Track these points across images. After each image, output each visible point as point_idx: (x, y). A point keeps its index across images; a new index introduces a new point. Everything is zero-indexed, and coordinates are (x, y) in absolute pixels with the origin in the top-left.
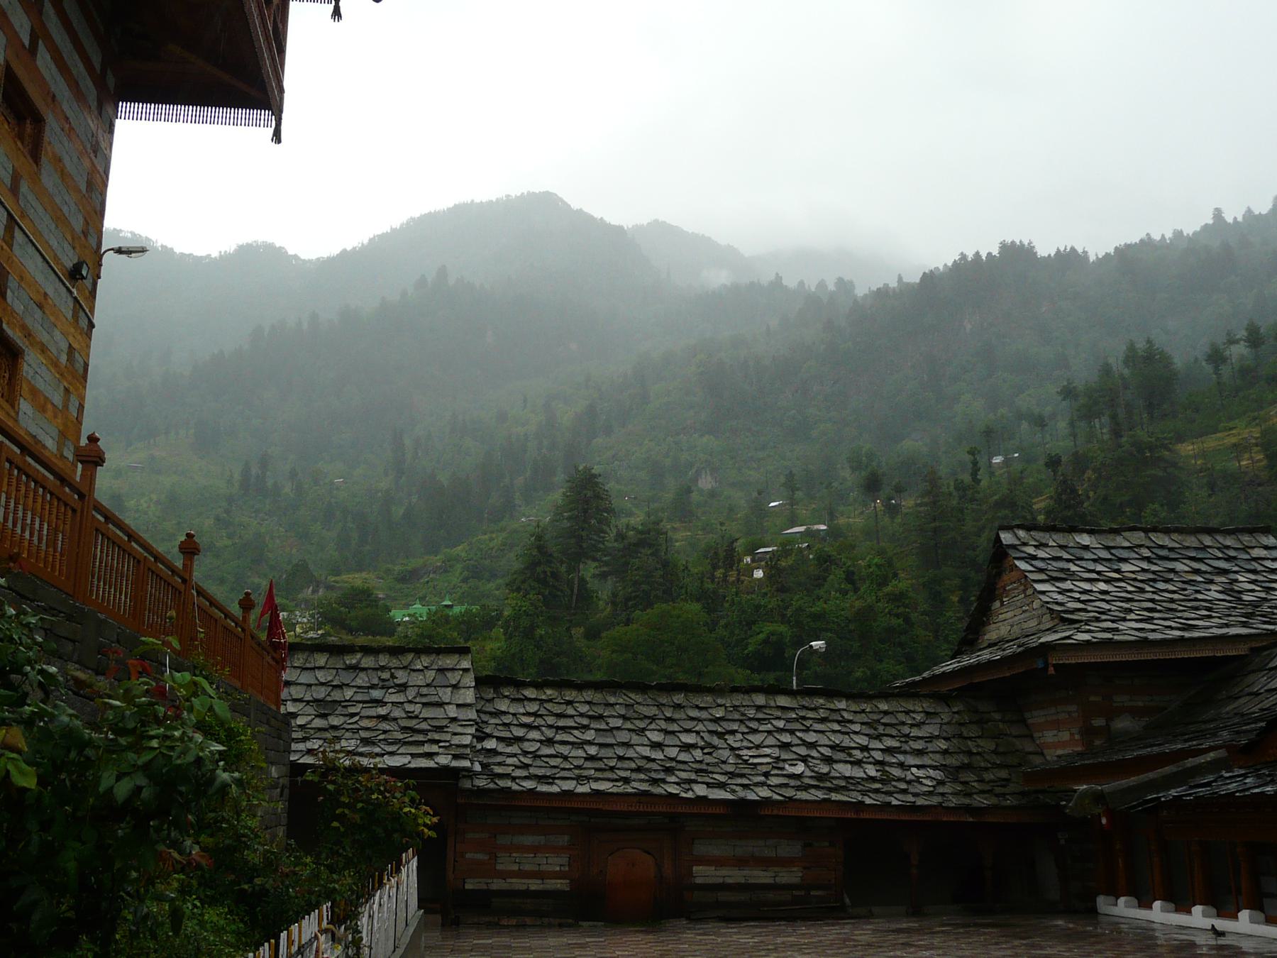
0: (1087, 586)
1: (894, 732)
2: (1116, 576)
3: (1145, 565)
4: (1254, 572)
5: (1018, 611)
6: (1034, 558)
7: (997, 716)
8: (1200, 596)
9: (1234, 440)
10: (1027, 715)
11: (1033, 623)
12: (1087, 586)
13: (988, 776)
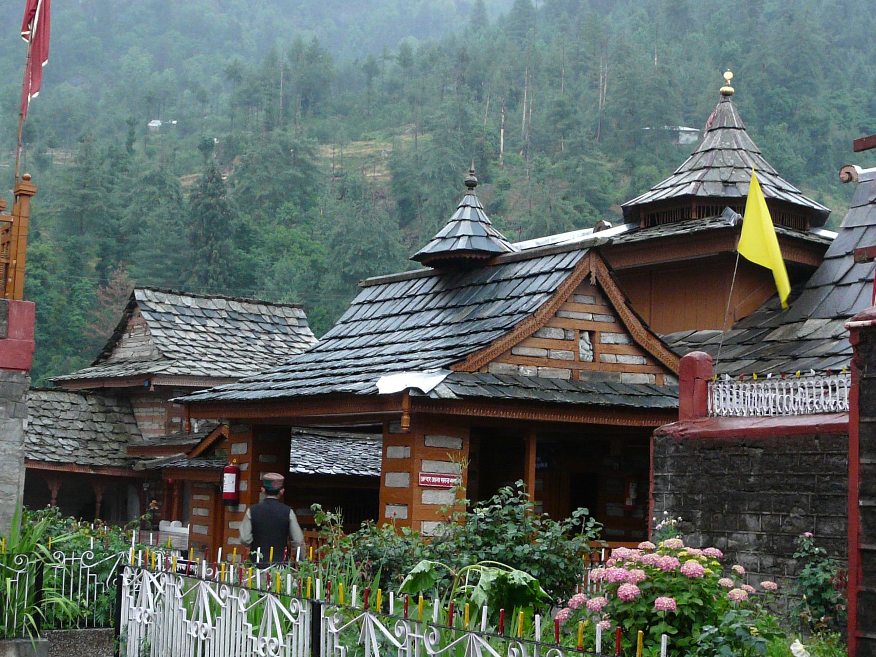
0: (182, 334)
1: (50, 415)
2: (203, 329)
3: (222, 323)
4: (286, 334)
5: (139, 344)
6: (155, 311)
7: (116, 409)
8: (249, 348)
9: (369, 151)
10: (135, 410)
11: (147, 354)
12: (182, 334)
13: (106, 447)
